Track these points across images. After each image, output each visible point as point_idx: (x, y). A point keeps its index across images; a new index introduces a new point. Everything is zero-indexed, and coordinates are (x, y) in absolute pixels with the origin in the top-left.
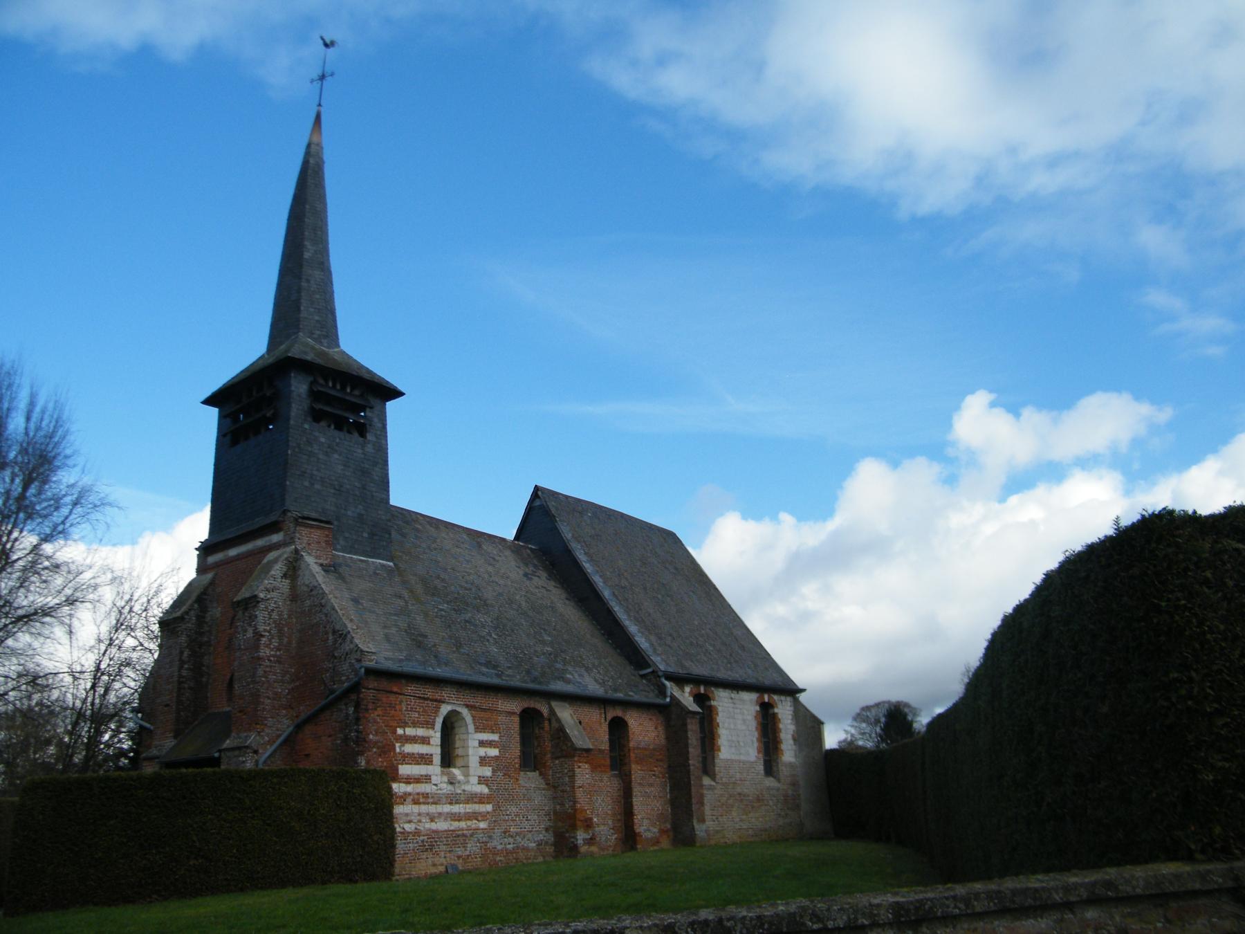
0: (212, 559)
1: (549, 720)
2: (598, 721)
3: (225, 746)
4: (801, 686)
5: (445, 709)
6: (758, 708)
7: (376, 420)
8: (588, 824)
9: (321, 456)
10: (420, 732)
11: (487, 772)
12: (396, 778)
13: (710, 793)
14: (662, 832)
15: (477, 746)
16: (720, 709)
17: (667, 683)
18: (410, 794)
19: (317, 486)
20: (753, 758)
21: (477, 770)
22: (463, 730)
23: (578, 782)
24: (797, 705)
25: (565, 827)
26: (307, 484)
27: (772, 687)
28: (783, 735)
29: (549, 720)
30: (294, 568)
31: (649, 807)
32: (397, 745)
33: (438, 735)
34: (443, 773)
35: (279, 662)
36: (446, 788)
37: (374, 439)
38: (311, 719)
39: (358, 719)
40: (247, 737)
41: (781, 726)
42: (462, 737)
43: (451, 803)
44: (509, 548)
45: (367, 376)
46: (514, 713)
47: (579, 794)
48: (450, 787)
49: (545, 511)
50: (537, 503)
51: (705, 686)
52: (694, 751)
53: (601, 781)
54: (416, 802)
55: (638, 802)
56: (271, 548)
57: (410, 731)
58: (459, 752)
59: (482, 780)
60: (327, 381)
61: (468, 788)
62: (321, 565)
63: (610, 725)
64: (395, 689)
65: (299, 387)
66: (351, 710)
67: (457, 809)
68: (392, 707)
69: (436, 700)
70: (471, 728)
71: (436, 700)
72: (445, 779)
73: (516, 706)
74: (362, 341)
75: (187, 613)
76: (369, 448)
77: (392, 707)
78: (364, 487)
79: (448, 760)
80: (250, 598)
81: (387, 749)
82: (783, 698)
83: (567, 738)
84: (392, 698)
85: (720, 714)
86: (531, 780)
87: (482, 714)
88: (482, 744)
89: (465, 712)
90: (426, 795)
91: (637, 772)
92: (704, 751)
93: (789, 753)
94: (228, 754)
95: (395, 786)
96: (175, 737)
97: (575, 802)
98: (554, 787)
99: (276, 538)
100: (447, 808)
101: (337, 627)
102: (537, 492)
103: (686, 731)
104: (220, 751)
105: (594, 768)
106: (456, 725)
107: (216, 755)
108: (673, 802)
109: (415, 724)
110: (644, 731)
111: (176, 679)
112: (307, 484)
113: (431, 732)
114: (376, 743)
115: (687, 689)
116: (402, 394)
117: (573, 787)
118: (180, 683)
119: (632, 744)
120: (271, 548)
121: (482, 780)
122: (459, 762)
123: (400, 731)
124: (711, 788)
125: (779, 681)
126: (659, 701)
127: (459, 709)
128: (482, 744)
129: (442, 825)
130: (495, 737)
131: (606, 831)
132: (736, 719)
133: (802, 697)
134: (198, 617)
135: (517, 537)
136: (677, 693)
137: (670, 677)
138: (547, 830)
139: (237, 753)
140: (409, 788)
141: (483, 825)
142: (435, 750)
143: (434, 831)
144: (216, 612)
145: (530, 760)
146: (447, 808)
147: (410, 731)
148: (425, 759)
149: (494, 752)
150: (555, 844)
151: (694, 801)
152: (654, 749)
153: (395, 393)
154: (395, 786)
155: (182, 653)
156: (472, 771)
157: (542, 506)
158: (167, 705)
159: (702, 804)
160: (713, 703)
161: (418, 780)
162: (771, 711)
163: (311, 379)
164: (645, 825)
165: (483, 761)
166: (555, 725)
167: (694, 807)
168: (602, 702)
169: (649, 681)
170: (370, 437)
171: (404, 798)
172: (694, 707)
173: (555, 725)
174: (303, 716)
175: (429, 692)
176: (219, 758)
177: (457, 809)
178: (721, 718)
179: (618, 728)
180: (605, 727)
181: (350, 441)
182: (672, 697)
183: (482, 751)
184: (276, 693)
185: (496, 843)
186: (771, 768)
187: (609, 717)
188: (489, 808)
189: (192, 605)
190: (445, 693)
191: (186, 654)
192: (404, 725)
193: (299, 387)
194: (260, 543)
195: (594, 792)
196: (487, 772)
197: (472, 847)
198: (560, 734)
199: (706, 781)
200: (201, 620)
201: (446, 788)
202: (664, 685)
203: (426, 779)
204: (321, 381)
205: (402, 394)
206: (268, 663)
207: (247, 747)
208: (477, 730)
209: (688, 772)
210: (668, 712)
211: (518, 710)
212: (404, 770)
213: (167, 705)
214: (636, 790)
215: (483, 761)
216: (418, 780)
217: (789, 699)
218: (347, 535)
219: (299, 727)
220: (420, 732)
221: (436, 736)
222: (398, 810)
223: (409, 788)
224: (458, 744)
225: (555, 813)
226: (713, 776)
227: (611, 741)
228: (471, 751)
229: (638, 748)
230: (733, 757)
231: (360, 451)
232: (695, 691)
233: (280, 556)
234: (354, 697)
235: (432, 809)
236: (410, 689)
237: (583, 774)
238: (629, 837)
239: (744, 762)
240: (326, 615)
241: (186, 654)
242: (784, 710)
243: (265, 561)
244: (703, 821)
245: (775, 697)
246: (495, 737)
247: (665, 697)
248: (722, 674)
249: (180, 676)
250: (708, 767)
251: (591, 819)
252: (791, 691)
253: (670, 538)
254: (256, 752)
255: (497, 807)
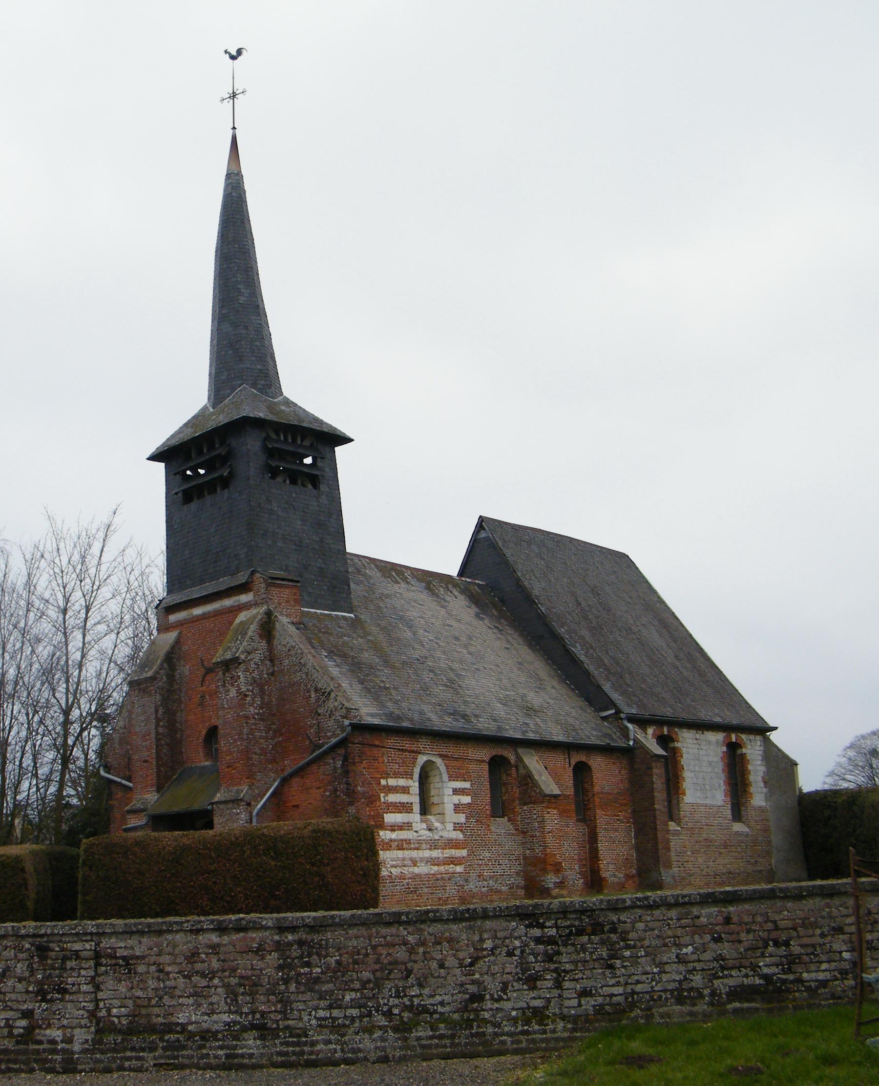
0: (173, 618)
1: (517, 767)
2: (563, 764)
3: (216, 799)
4: (772, 724)
5: (422, 759)
6: (724, 749)
7: (327, 470)
8: (558, 868)
9: (280, 513)
10: (402, 782)
11: (461, 818)
12: (381, 826)
13: (677, 838)
14: (628, 877)
15: (451, 794)
16: (684, 750)
17: (630, 726)
18: (395, 840)
19: (280, 544)
20: (720, 803)
21: (453, 818)
22: (437, 779)
23: (548, 828)
24: (767, 742)
25: (534, 871)
26: (270, 542)
27: (742, 728)
28: (752, 778)
29: (517, 767)
30: (267, 629)
31: (615, 849)
32: (382, 795)
33: (417, 784)
34: (422, 821)
35: (262, 720)
36: (425, 834)
37: (327, 490)
38: (300, 772)
39: (347, 772)
40: (238, 792)
41: (750, 767)
42: (437, 785)
43: (430, 849)
44: (456, 585)
45: (315, 426)
46: (484, 761)
47: (549, 839)
48: (427, 832)
49: (492, 545)
50: (483, 535)
51: (668, 728)
52: (660, 795)
53: (567, 826)
54: (400, 848)
55: (602, 846)
56: (241, 608)
57: (392, 782)
58: (435, 800)
59: (457, 827)
60: (278, 436)
61: (445, 834)
62: (293, 623)
63: (574, 769)
64: (377, 743)
65: (251, 445)
66: (339, 763)
67: (435, 854)
68: (376, 759)
69: (413, 752)
70: (445, 777)
71: (413, 752)
72: (424, 826)
73: (485, 754)
74: (307, 382)
75: (157, 672)
76: (324, 500)
77: (376, 759)
78: (322, 541)
79: (424, 810)
80: (231, 660)
81: (372, 799)
82: (752, 737)
83: (535, 784)
84: (375, 751)
85: (685, 756)
86: (501, 826)
87: (455, 763)
88: (456, 792)
89: (439, 761)
90: (408, 842)
91: (602, 818)
92: (669, 794)
93: (758, 797)
94: (221, 806)
95: (381, 833)
96: (158, 791)
97: (545, 847)
98: (523, 832)
99: (245, 598)
100: (427, 854)
101: (320, 686)
102: (482, 523)
103: (651, 775)
104: (212, 804)
105: (563, 813)
106: (431, 774)
107: (209, 807)
108: (638, 848)
109: (396, 775)
110: (606, 776)
111: (153, 735)
112: (270, 542)
113: (410, 782)
114: (364, 793)
115: (650, 731)
116: (349, 440)
117: (543, 832)
118: (158, 740)
119: (597, 789)
120: (241, 608)
121: (457, 827)
122: (435, 810)
123: (383, 782)
124: (676, 833)
125: (747, 721)
126: (621, 743)
127: (434, 759)
128: (456, 792)
129: (422, 869)
130: (467, 785)
131: (574, 874)
132: (701, 760)
133: (773, 736)
134: (167, 675)
135: (461, 573)
136: (640, 736)
137: (632, 719)
138: (517, 874)
139: (230, 805)
140: (394, 835)
141: (459, 869)
142: (414, 799)
143: (417, 875)
144: (185, 669)
145: (500, 808)
146: (427, 854)
147: (392, 782)
148: (405, 808)
149: (466, 799)
150: (526, 888)
151: (660, 846)
152: (618, 794)
153: (345, 440)
154: (381, 833)
155: (157, 711)
156: (447, 819)
157: (487, 539)
158: (146, 761)
159: (668, 849)
160: (676, 745)
161: (401, 827)
162: (739, 752)
163: (264, 435)
164: (609, 870)
165: (458, 808)
166: (522, 771)
167: (662, 852)
168: (566, 748)
169: (611, 723)
170: (323, 488)
171: (388, 845)
172: (660, 751)
173: (522, 771)
174: (289, 770)
175: (407, 744)
176: (212, 810)
177: (435, 854)
178: (686, 760)
179: (581, 771)
180: (569, 773)
181: (304, 494)
182: (636, 740)
183: (456, 799)
184: (262, 749)
185: (472, 886)
186: (739, 813)
187: (573, 763)
188: (464, 853)
189: (162, 665)
190: (422, 744)
191: (161, 711)
192: (387, 776)
193: (251, 445)
194: (228, 602)
195: (560, 836)
196: (461, 818)
197: (451, 890)
198: (527, 780)
199: (672, 826)
200: (171, 678)
201: (425, 834)
202: (627, 728)
203: (408, 826)
204: (274, 436)
205: (349, 440)
206: (252, 721)
207: (241, 800)
208: (452, 778)
209: (655, 817)
210: (629, 754)
211: (487, 759)
212: (390, 818)
213: (146, 761)
214: (601, 834)
215: (458, 808)
216: (401, 827)
217: (758, 738)
218: (310, 590)
219: (285, 781)
220: (402, 782)
221: (414, 785)
222: (383, 855)
223: (394, 835)
224: (433, 792)
225: (525, 858)
226: (678, 822)
227: (576, 785)
228: (446, 799)
229: (602, 793)
230: (699, 801)
231: (315, 503)
232: (658, 733)
233: (254, 617)
234: (342, 751)
235: (414, 854)
236: (391, 741)
237: (552, 819)
238: (594, 881)
239: (711, 807)
240: (307, 674)
241: (161, 711)
242: (753, 750)
243: (238, 621)
244: (669, 866)
245: (743, 736)
246: (467, 785)
247: (629, 740)
248: (684, 716)
249: (157, 733)
250: (672, 814)
251: (560, 863)
252: (762, 730)
253: (622, 561)
254: (249, 804)
255: (471, 853)
